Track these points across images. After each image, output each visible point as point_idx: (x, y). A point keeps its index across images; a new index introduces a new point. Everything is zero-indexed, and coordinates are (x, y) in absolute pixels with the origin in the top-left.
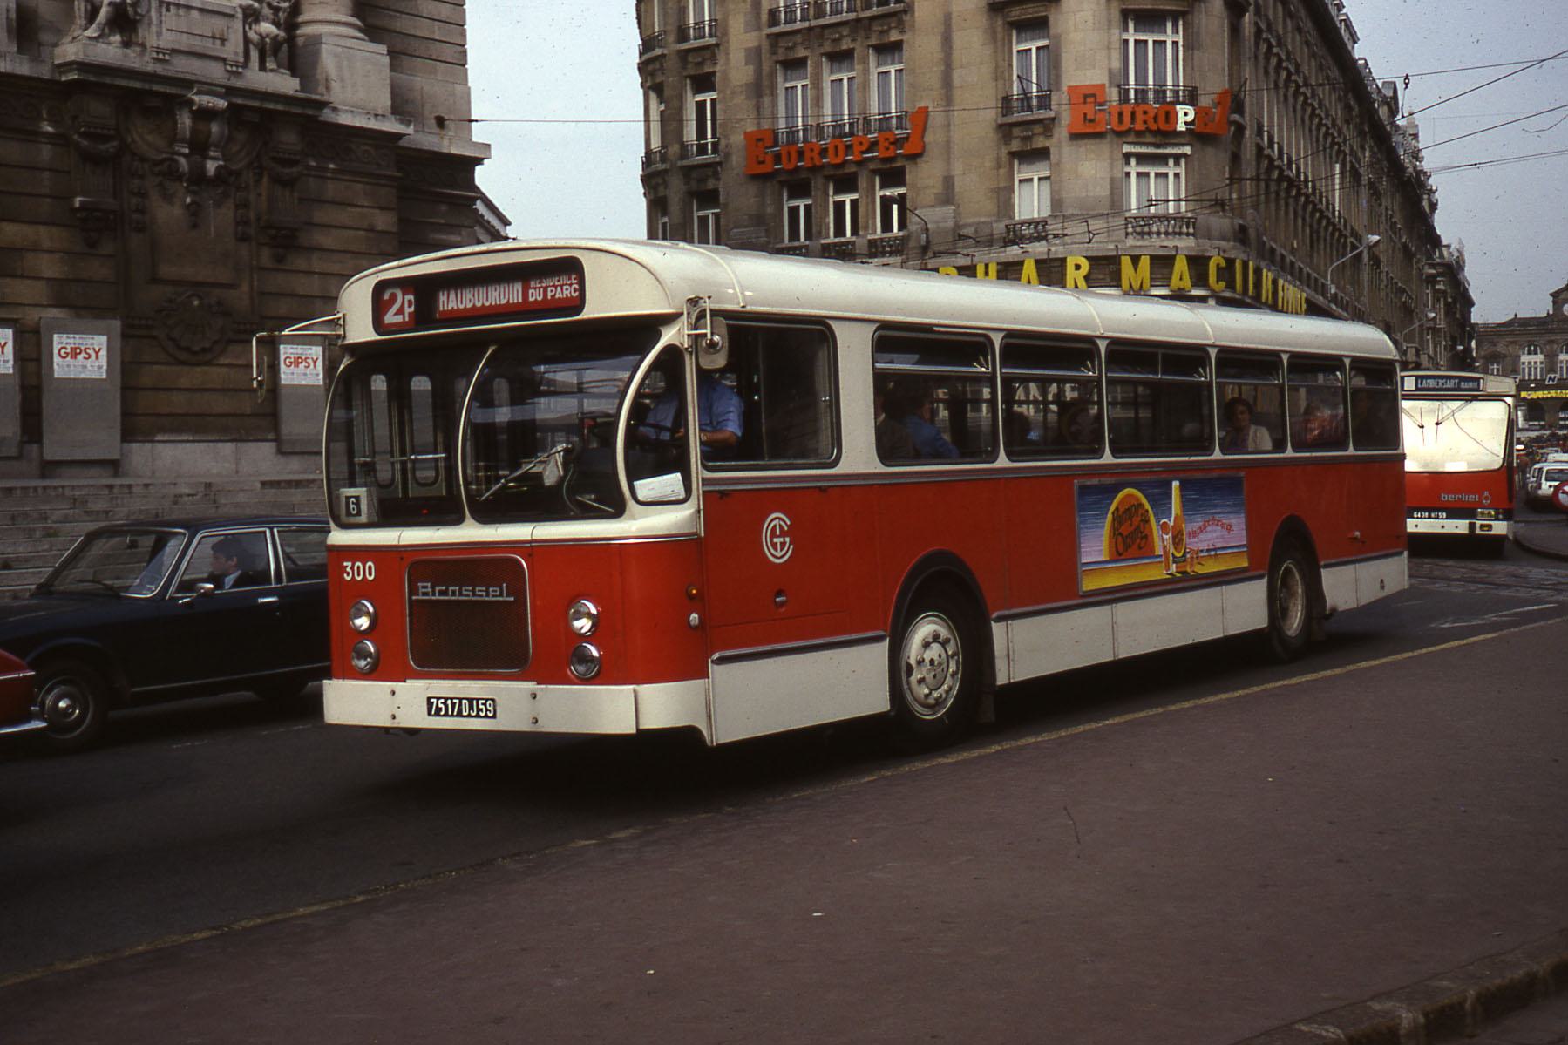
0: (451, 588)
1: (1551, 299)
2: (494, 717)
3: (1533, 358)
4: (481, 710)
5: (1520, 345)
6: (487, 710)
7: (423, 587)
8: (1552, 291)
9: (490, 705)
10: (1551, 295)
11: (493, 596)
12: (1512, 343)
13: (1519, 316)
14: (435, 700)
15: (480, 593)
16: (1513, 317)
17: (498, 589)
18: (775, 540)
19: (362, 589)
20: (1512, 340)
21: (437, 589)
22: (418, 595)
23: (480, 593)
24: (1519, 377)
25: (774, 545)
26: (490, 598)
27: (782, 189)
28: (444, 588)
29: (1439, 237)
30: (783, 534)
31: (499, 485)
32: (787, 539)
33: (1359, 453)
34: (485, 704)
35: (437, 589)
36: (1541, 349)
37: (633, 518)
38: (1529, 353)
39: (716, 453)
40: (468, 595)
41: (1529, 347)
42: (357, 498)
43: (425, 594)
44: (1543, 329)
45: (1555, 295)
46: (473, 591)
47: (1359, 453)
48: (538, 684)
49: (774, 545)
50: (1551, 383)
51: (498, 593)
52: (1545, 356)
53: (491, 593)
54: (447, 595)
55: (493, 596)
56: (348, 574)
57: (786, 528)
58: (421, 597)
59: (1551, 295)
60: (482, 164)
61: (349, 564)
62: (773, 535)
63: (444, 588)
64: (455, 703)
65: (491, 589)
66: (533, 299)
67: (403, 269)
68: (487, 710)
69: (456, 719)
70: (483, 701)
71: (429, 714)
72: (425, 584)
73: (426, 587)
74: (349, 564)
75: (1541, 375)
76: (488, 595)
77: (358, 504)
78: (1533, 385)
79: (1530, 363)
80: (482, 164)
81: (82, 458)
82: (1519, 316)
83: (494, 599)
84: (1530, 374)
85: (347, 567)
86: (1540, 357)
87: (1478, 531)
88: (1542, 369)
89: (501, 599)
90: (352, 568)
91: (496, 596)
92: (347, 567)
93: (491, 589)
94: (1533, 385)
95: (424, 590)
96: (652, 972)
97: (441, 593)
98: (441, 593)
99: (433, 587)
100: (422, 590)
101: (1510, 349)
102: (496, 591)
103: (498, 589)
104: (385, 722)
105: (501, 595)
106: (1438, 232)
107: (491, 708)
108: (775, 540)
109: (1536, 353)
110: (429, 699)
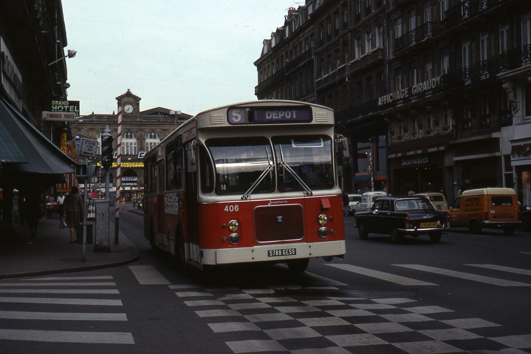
1: (117, 101)
2: (295, 254)
3: (130, 141)
5: (97, 131)
6: (292, 252)
8: (116, 97)
10: (116, 98)
12: (91, 129)
13: (95, 114)
14: (275, 251)
16: (91, 113)
20: (91, 127)
34: (291, 251)
36: (158, 134)
38: (127, 137)
39: (500, 157)
41: (127, 133)
44: (112, 121)
45: (119, 99)
48: (307, 243)
52: (137, 139)
59: (116, 98)
66: (270, 117)
69: (274, 257)
71: (295, 249)
75: (135, 152)
78: (129, 159)
79: (127, 143)
82: (95, 114)
84: (127, 151)
86: (134, 141)
88: (135, 148)
94: (129, 159)
101: (90, 134)
104: (250, 260)
107: (294, 251)
109: (131, 137)
110: (269, 251)
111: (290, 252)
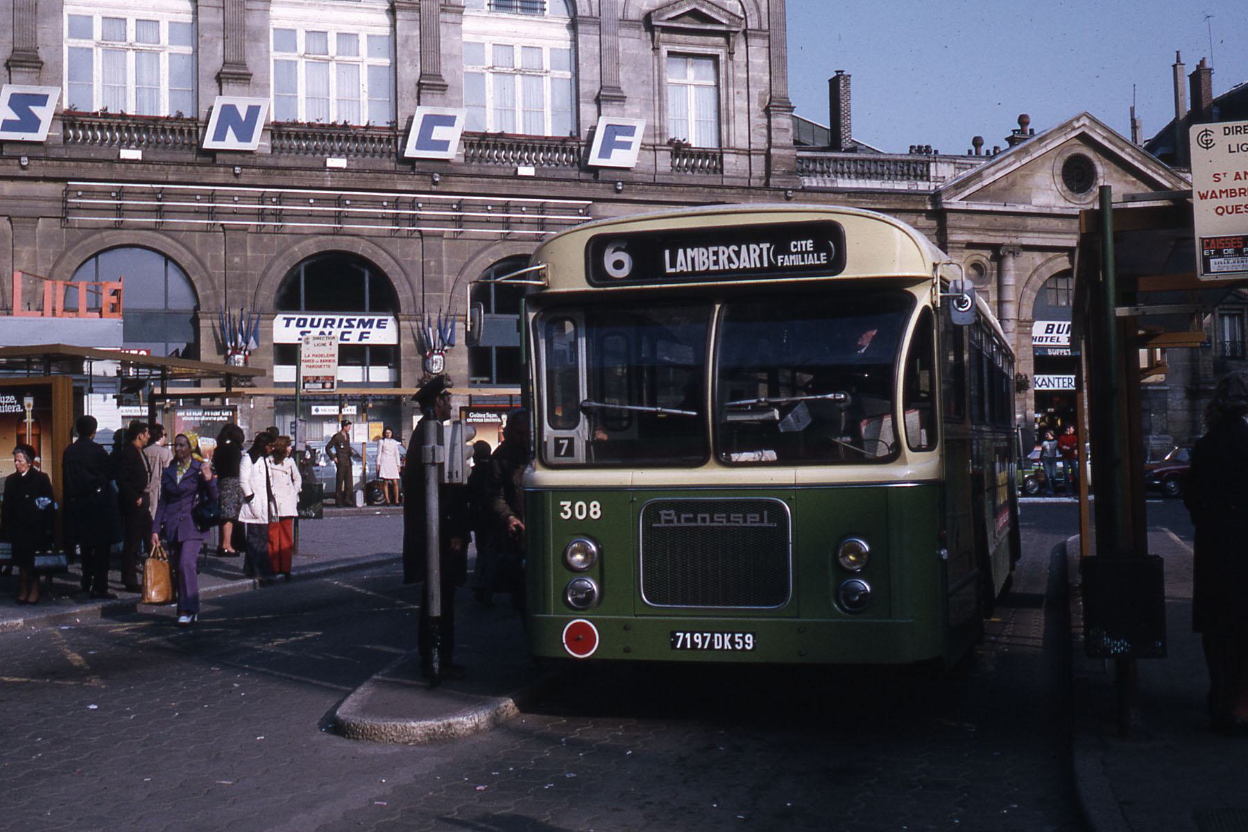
6: (745, 643)
9: (749, 638)
10: (1006, 139)
15: (736, 520)
17: (757, 516)
19: (585, 529)
21: (683, 516)
22: (660, 522)
24: (53, 93)
27: (1170, 200)
31: (654, 409)
34: (743, 638)
35: (683, 516)
37: (905, 463)
50: (231, 142)
51: (758, 519)
56: (566, 513)
58: (663, 524)
59: (1006, 139)
60: (1124, 196)
61: (569, 504)
63: (691, 516)
64: (706, 637)
68: (745, 643)
70: (741, 635)
73: (670, 515)
74: (569, 504)
76: (745, 521)
80: (1124, 196)
81: (402, 377)
85: (565, 506)
87: (707, 516)
89: (761, 525)
90: (572, 508)
91: (755, 522)
92: (565, 506)
95: (708, 520)
96: (1016, 806)
97: (687, 520)
98: (687, 520)
102: (755, 518)
111: (738, 643)
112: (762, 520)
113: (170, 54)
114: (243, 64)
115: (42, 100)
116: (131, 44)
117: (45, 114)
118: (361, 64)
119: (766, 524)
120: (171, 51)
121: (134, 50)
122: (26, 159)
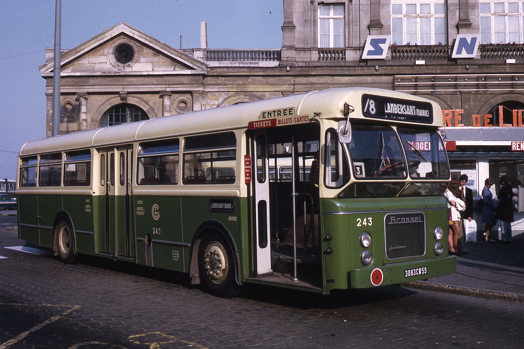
0: (402, 219)
4: (423, 271)
6: (425, 271)
7: (393, 219)
11: (417, 221)
18: (155, 213)
23: (412, 220)
25: (155, 214)
26: (416, 221)
28: (400, 219)
29: (236, 139)
30: (157, 211)
32: (158, 213)
33: (234, 191)
34: (424, 269)
35: (398, 219)
40: (412, 221)
42: (361, 167)
43: (393, 221)
46: (410, 219)
47: (234, 191)
49: (155, 214)
53: (416, 220)
54: (401, 221)
55: (417, 221)
57: (158, 209)
62: (155, 211)
63: (400, 219)
65: (416, 218)
67: (108, 79)
68: (425, 271)
72: (393, 217)
76: (415, 221)
77: (361, 170)
83: (417, 222)
93: (416, 218)
99: (396, 219)
100: (391, 220)
103: (418, 218)
105: (419, 220)
106: (245, 137)
107: (426, 270)
108: (155, 213)
112: (419, 220)
113: (435, 18)
114: (468, 20)
115: (384, 41)
116: (418, 15)
117: (385, 47)
118: (520, 16)
119: (420, 221)
120: (435, 16)
121: (419, 17)
122: (378, 66)
